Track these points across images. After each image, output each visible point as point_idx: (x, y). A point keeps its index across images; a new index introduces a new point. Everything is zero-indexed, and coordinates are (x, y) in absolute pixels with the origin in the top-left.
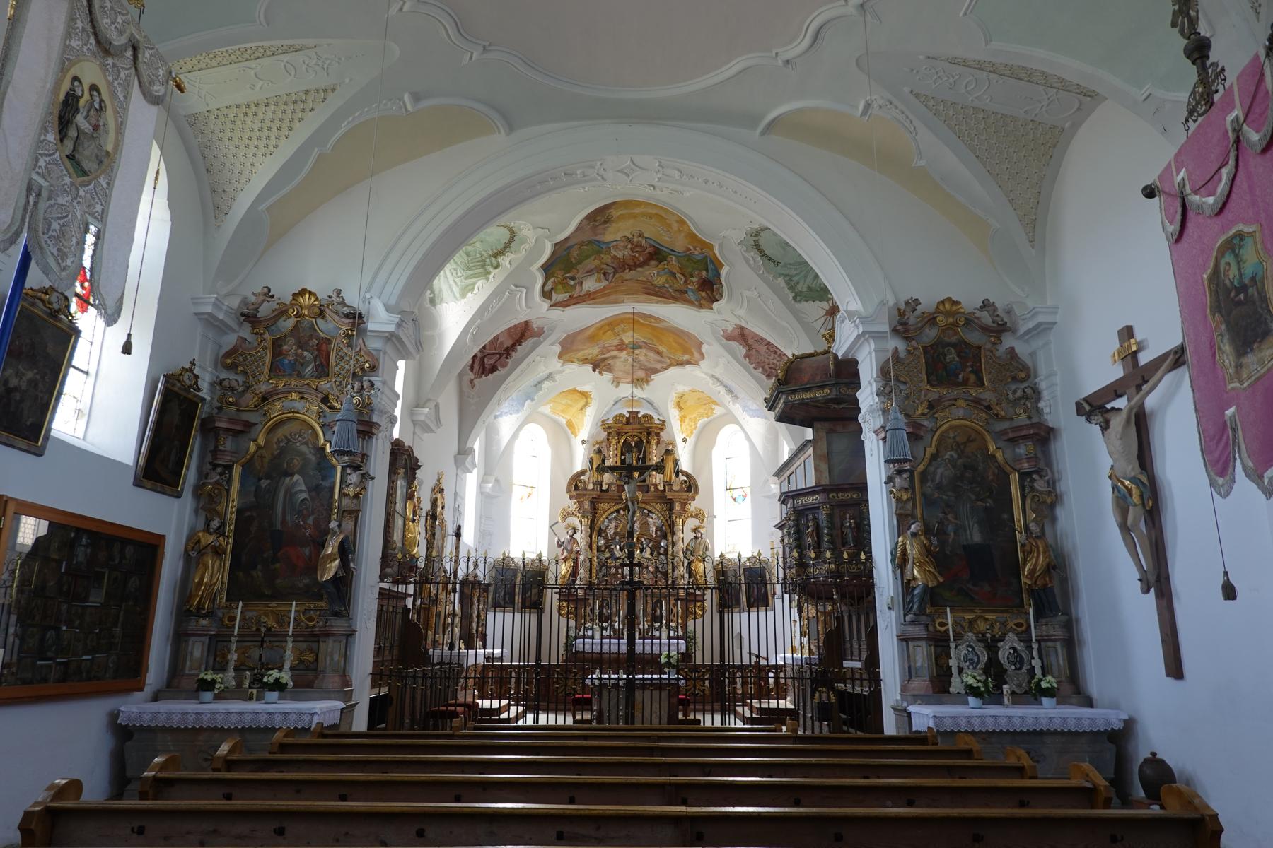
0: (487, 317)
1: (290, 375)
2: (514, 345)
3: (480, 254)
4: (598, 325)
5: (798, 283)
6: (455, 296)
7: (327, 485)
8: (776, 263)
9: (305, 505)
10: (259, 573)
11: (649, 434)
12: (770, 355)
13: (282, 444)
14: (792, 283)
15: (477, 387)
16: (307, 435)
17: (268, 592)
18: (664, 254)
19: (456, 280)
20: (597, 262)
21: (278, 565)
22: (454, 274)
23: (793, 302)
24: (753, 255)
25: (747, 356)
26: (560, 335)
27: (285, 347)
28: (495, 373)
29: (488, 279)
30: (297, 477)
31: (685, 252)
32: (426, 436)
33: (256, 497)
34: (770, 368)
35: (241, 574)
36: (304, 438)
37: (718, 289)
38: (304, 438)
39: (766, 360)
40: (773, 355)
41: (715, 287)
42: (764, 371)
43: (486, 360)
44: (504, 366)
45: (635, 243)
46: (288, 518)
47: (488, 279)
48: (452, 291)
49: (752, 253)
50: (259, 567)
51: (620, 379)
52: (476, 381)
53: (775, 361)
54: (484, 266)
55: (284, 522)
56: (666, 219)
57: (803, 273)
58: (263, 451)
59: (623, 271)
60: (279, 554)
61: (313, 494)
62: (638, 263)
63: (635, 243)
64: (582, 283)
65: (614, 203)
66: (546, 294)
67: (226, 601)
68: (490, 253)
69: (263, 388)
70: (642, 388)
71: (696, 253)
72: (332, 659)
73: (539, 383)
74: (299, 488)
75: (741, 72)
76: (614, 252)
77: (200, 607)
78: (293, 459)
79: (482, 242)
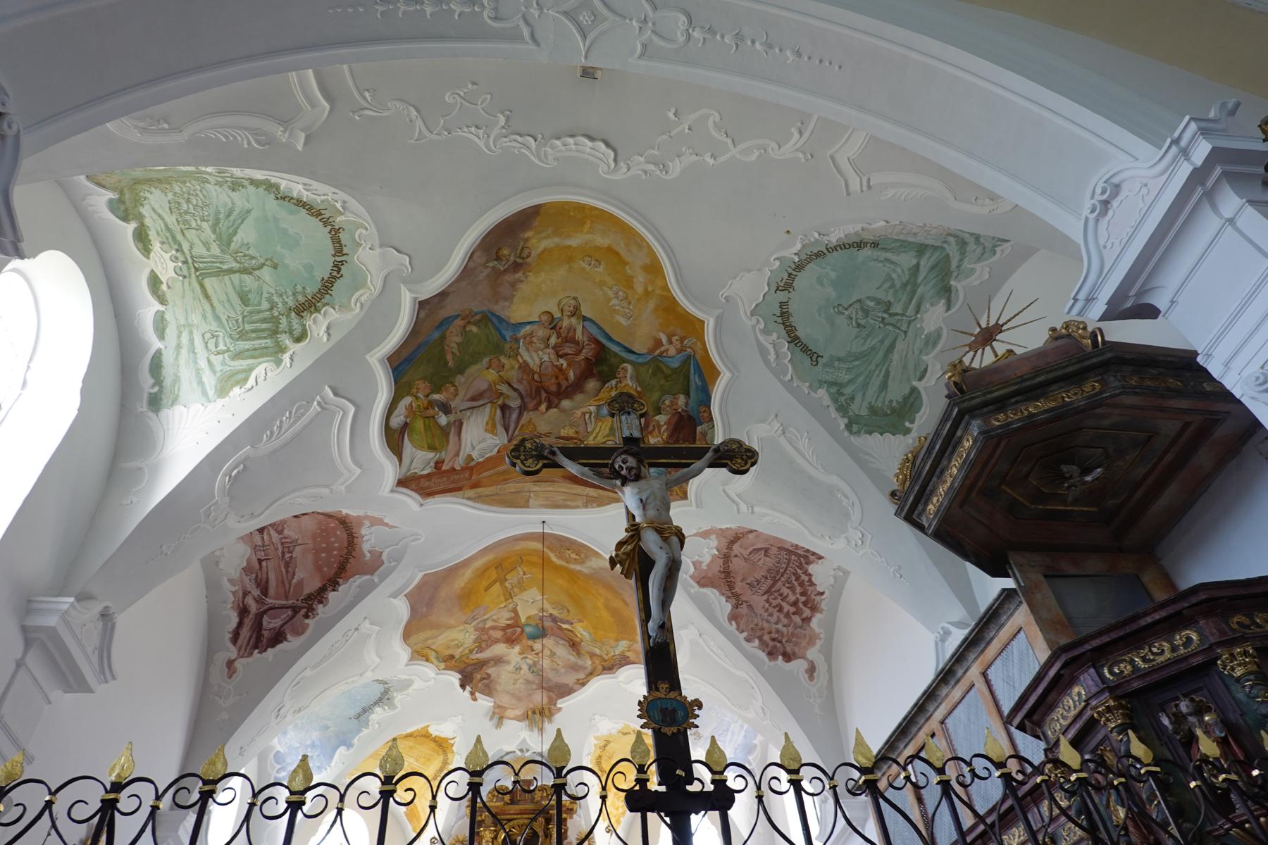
0: (265, 446)
2: (323, 590)
3: (270, 300)
4: (479, 563)
5: (853, 398)
6: (205, 393)
8: (814, 357)
12: (771, 615)
14: (842, 399)
15: (238, 677)
18: (613, 361)
19: (212, 357)
20: (492, 375)
22: (211, 345)
23: (846, 434)
24: (778, 336)
25: (733, 617)
26: (407, 575)
28: (280, 647)
29: (279, 363)
31: (651, 351)
32: (66, 700)
34: (773, 640)
39: (766, 625)
40: (776, 614)
41: (699, 429)
42: (763, 644)
43: (266, 619)
44: (298, 632)
45: (564, 332)
47: (279, 363)
48: (201, 383)
49: (775, 336)
51: (505, 709)
52: (238, 664)
53: (780, 626)
54: (275, 332)
56: (625, 263)
57: (861, 379)
59: (536, 408)
62: (564, 384)
63: (564, 332)
64: (459, 425)
65: (535, 211)
66: (394, 439)
68: (291, 303)
71: (672, 351)
73: (365, 711)
76: (525, 355)
79: (275, 267)
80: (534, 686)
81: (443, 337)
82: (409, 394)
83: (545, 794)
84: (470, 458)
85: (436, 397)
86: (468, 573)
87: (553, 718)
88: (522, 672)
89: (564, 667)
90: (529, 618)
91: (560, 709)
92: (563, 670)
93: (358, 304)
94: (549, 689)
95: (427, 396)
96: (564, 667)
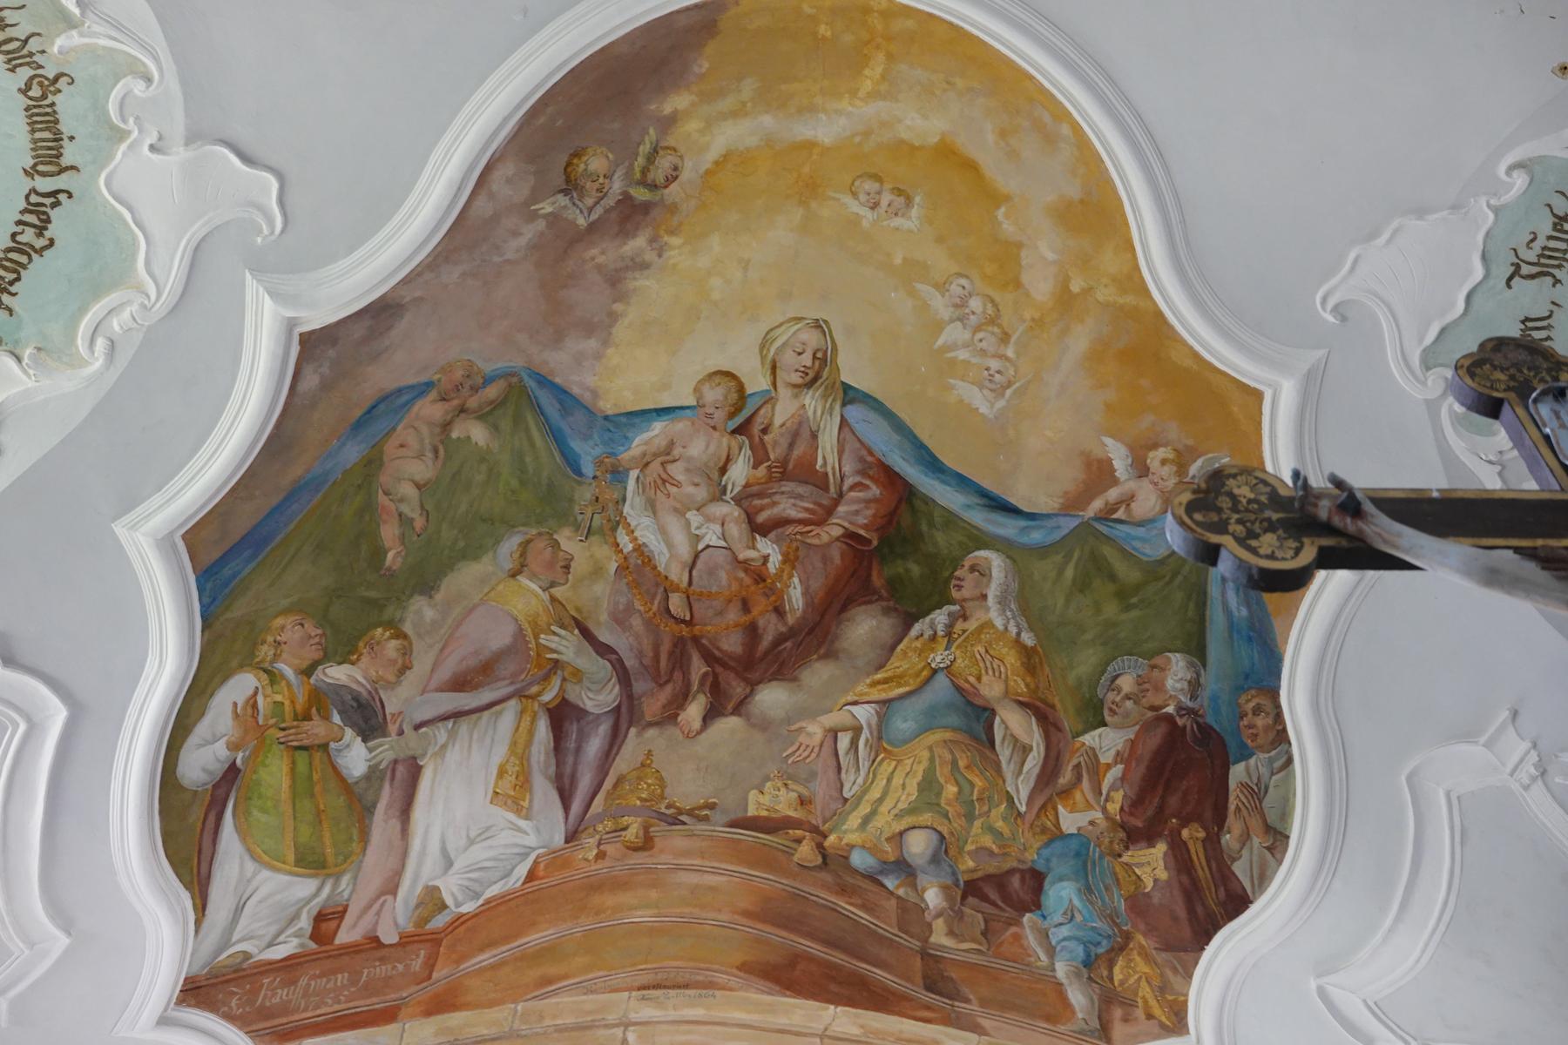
20: (527, 597)
31: (1073, 504)
37: (1257, 793)
56: (995, 198)
62: (771, 628)
72: (1011, 610)
75: (192, 266)
82: (248, 662)
84: (432, 900)
85: (337, 674)
93: (101, 343)
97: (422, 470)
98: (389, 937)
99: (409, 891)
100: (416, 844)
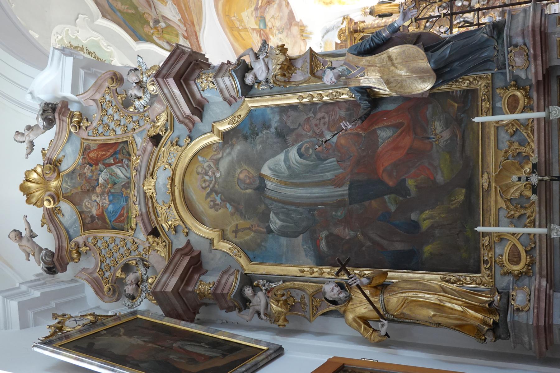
1: (127, 199)
4: (232, 39)
7: (277, 118)
9: (307, 149)
10: (424, 216)
11: (356, 31)
13: (218, 201)
16: (205, 162)
17: (460, 196)
21: (411, 183)
27: (94, 212)
30: (266, 171)
33: (295, 235)
35: (428, 249)
36: (209, 166)
38: (209, 166)
46: (329, 175)
50: (414, 217)
55: (336, 182)
58: (229, 229)
60: (391, 183)
61: (290, 139)
67: (478, 271)
69: (141, 236)
70: (311, 33)
74: (282, 164)
75: (95, 31)
77: (490, 309)
78: (239, 179)
80: (289, 33)
81: (120, 11)
82: (151, 36)
83: (343, 35)
84: (180, 20)
85: (151, 24)
86: (236, 45)
87: (305, 25)
88: (282, 38)
89: (280, 13)
90: (256, 23)
91: (301, 20)
92: (281, 14)
93: (108, 47)
94: (291, 25)
95: (152, 28)
96: (280, 13)
97: (120, 4)
98: (185, 29)
99: (179, 23)
100: (173, 20)
